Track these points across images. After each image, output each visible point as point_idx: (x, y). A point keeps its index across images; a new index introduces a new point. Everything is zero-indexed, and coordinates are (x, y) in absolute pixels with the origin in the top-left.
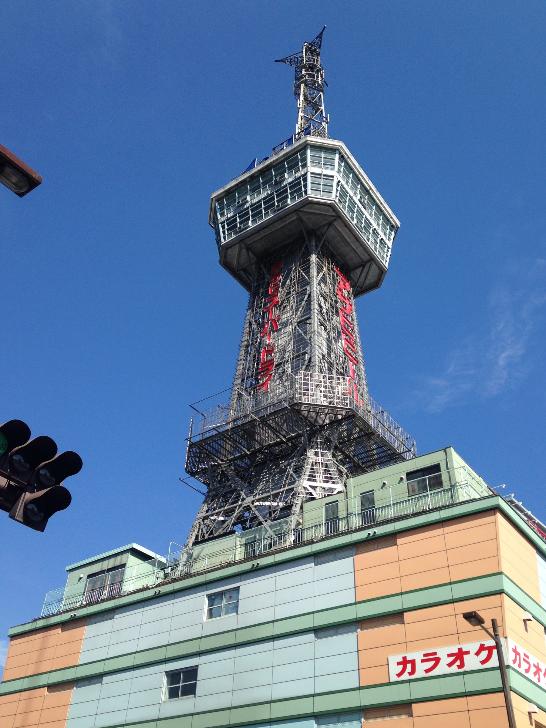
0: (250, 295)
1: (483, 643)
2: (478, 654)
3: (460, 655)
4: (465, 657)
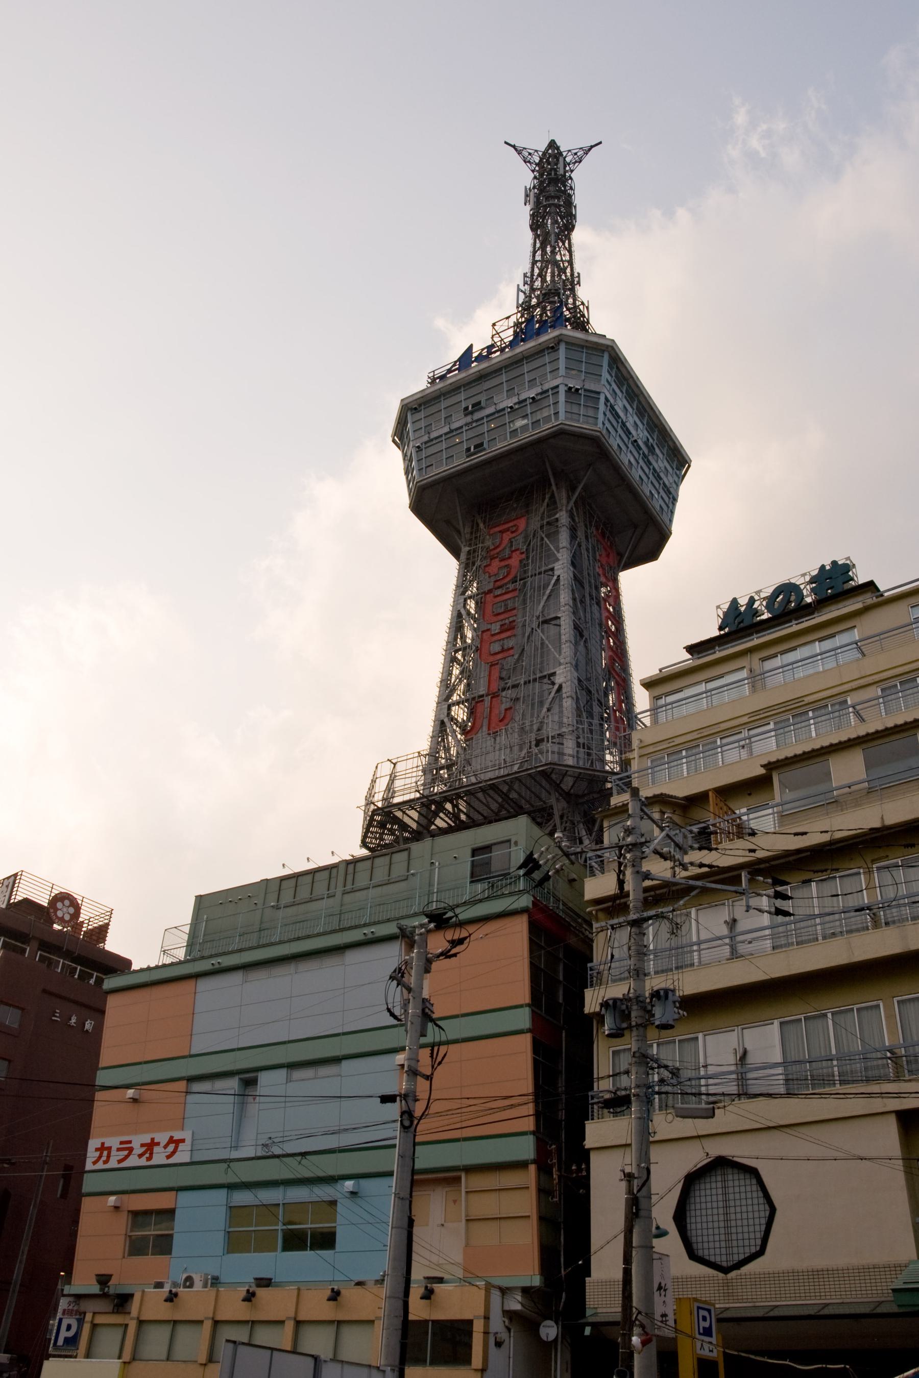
0: (459, 565)
1: (172, 1135)
2: (165, 1147)
3: (150, 1146)
4: (156, 1149)
